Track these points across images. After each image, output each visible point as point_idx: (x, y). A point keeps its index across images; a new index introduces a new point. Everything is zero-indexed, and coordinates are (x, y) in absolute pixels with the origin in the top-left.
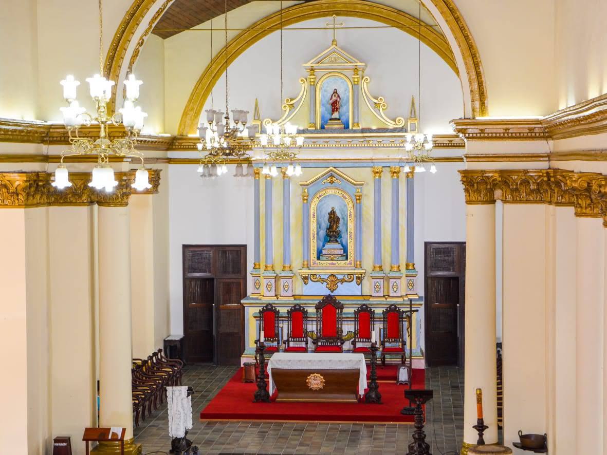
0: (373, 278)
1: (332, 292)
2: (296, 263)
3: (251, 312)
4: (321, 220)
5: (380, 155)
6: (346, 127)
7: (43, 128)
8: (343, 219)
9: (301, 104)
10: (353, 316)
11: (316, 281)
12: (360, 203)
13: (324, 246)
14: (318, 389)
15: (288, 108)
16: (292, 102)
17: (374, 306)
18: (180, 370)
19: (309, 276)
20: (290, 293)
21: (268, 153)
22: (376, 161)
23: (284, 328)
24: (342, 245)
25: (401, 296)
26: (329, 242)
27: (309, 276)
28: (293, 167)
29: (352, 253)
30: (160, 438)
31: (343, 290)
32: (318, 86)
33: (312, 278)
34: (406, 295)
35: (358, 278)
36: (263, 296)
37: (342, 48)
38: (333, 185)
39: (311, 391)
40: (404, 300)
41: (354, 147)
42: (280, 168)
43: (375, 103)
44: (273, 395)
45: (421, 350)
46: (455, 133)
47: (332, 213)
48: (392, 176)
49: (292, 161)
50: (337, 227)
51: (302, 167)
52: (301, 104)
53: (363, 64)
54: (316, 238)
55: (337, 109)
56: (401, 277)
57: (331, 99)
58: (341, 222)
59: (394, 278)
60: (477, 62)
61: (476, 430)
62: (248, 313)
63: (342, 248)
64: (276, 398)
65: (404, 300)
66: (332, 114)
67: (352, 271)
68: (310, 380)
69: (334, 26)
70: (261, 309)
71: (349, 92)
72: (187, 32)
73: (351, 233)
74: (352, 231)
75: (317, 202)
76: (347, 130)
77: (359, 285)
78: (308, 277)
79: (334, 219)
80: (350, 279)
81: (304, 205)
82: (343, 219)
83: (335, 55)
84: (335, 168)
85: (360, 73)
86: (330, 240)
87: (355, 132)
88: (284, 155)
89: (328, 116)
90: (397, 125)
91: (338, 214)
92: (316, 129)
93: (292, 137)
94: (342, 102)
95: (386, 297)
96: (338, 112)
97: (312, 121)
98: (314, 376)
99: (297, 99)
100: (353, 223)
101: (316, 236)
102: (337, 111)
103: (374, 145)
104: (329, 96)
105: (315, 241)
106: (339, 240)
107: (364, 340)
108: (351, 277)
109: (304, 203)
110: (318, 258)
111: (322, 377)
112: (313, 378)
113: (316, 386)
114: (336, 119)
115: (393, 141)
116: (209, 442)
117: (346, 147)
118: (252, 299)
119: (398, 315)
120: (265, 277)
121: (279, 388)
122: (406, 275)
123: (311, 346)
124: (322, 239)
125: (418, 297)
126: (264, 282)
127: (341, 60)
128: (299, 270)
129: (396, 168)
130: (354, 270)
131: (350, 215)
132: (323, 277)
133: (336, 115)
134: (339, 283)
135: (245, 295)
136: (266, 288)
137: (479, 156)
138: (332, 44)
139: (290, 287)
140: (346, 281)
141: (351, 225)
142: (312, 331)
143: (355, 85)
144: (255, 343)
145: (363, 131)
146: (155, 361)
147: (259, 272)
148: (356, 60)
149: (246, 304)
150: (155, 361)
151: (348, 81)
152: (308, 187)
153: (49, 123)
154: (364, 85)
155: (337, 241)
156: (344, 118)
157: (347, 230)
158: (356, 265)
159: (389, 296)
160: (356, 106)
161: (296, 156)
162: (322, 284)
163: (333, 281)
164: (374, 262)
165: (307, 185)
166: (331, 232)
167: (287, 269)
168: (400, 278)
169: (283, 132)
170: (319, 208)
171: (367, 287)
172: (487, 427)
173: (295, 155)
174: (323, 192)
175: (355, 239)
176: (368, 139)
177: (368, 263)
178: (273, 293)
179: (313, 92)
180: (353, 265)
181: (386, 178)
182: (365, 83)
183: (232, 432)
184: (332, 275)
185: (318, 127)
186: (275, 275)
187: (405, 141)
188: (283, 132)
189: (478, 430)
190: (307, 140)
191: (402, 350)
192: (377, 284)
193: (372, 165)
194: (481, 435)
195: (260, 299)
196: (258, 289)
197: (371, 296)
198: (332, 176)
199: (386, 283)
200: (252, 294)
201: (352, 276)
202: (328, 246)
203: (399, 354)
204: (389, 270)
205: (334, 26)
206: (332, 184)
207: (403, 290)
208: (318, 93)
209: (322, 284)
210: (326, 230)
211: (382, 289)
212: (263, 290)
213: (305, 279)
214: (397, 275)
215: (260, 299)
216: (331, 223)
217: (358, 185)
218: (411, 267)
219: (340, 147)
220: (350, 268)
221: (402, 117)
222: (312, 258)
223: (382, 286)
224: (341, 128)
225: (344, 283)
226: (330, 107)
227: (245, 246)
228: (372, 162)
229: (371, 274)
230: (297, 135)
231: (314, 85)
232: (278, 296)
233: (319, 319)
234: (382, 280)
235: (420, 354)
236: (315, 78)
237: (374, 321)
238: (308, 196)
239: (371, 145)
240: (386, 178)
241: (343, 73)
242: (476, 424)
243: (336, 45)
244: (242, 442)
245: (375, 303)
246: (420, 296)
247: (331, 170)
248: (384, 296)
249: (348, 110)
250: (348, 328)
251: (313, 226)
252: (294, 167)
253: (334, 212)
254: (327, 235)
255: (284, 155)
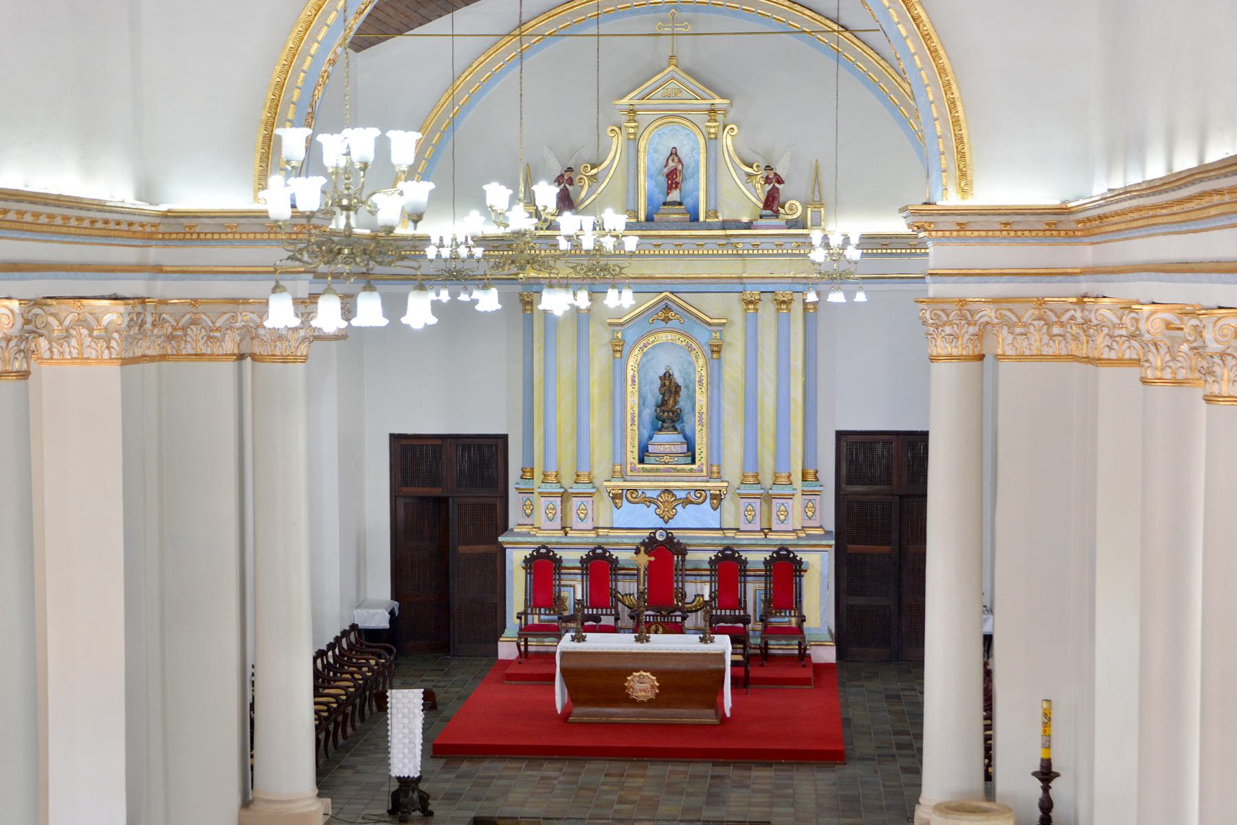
0: (743, 497)
1: (666, 522)
2: (601, 469)
3: (516, 559)
4: (646, 389)
5: (756, 268)
6: (695, 218)
7: (158, 216)
8: (687, 387)
9: (610, 175)
10: (579, 565)
11: (637, 503)
12: (719, 359)
13: (651, 438)
14: (645, 700)
15: (587, 182)
16: (594, 171)
17: (745, 548)
18: (391, 664)
19: (625, 492)
20: (589, 524)
21: (571, 265)
22: (748, 281)
23: (574, 590)
24: (685, 437)
25: (794, 531)
26: (660, 430)
27: (625, 492)
28: (616, 291)
29: (704, 450)
30: (361, 790)
31: (686, 518)
32: (642, 144)
33: (629, 496)
34: (803, 527)
35: (713, 497)
36: (539, 528)
37: (688, 72)
38: (668, 325)
39: (634, 702)
40: (598, 536)
41: (708, 255)
42: (774, 292)
43: (749, 175)
44: (564, 708)
45: (830, 631)
46: (910, 231)
47: (667, 377)
48: (746, 310)
49: (616, 281)
50: (676, 402)
51: (634, 292)
52: (610, 175)
53: (727, 101)
54: (636, 423)
55: (677, 183)
56: (793, 495)
57: (666, 166)
58: (683, 392)
59: (782, 497)
60: (953, 98)
61: (1037, 779)
62: (512, 561)
63: (684, 441)
64: (568, 717)
65: (598, 536)
66: (668, 194)
67: (703, 484)
68: (632, 683)
69: (673, 30)
70: (767, 555)
71: (699, 153)
72: (398, 38)
73: (701, 414)
74: (704, 410)
75: (640, 356)
76: (695, 223)
77: (715, 509)
78: (622, 494)
79: (670, 388)
80: (699, 498)
81: (614, 363)
82: (687, 387)
83: (674, 85)
84: (672, 293)
85: (720, 117)
86: (662, 426)
87: (710, 227)
88: (601, 270)
89: (660, 198)
90: (788, 214)
91: (678, 379)
92: (638, 221)
93: (617, 237)
94: (687, 172)
95: (766, 531)
96: (678, 191)
97: (631, 207)
98: (639, 676)
99: (603, 166)
100: (705, 395)
101: (636, 419)
102: (676, 187)
103: (746, 252)
104: (663, 160)
105: (636, 428)
106: (679, 427)
107: (543, 610)
108: (701, 494)
109: (614, 358)
110: (641, 461)
111: (654, 678)
112: (638, 679)
113: (643, 694)
114: (674, 203)
115: (781, 245)
116: (452, 797)
117: (693, 255)
118: (519, 534)
119: (736, 566)
120: (543, 495)
121: (576, 695)
122: (803, 491)
123: (626, 621)
124: (648, 426)
125: (823, 533)
126: (541, 503)
127: (685, 95)
128: (605, 481)
129: (783, 292)
130: (708, 482)
131: (700, 381)
132: (649, 494)
133: (675, 195)
134: (680, 505)
135: (505, 528)
136: (743, 517)
137: (1069, 270)
138: (669, 65)
139: (590, 511)
140: (692, 503)
141: (701, 398)
142: (630, 595)
143: (712, 140)
144: (518, 618)
145: (725, 225)
146: (345, 646)
147: (533, 484)
148: (714, 95)
149: (509, 543)
150: (345, 646)
151: (697, 131)
152: (623, 328)
153: (163, 208)
154: (727, 140)
155: (675, 429)
156: (688, 201)
157: (694, 409)
158: (712, 473)
159: (770, 529)
160: (712, 178)
161: (623, 271)
162: (648, 507)
163: (668, 500)
164: (744, 468)
165: (621, 325)
166: (664, 412)
167: (584, 479)
168: (790, 497)
169: (598, 226)
170: (641, 367)
171: (731, 513)
172: (1057, 775)
173: (621, 268)
174: (651, 339)
175: (710, 427)
176: (734, 240)
177: (732, 469)
178: (558, 525)
179: (632, 152)
180: (705, 473)
181: (767, 311)
182: (729, 137)
183: (493, 777)
184: (667, 491)
185: (642, 217)
186: (562, 490)
187: (811, 246)
188: (598, 226)
189: (1042, 780)
190: (644, 241)
191: (799, 631)
192: (750, 507)
193: (740, 288)
194: (1046, 789)
195: (535, 536)
196: (528, 516)
197: (738, 530)
198: (667, 308)
199: (765, 507)
200: (519, 525)
201: (703, 492)
202: (660, 437)
203: (793, 639)
204: (771, 482)
205: (673, 30)
206: (667, 323)
207: (796, 521)
208: (641, 155)
209: (648, 507)
210: (654, 409)
211: (758, 517)
212: (540, 519)
213: (616, 497)
214: (787, 491)
215: (535, 536)
216: (664, 394)
217: (716, 325)
218: (810, 477)
219: (683, 255)
220: (700, 479)
221: (794, 199)
222: (630, 459)
223: (758, 512)
224: (683, 221)
225: (690, 506)
226: (663, 181)
227: (504, 438)
228: (741, 284)
229: (738, 489)
230: (627, 233)
231: (635, 139)
232: (567, 529)
233: (585, 572)
234: (758, 501)
235: (829, 638)
236: (637, 127)
237: (745, 576)
238: (622, 345)
239: (740, 252)
240: (767, 311)
241: (688, 118)
242: (1037, 768)
243: (676, 66)
244: (512, 797)
245: (745, 542)
246: (827, 529)
247: (666, 298)
248: (762, 530)
249: (699, 189)
250: (700, 589)
251: (632, 400)
252: (620, 292)
253: (670, 375)
254: (658, 418)
255: (601, 270)
